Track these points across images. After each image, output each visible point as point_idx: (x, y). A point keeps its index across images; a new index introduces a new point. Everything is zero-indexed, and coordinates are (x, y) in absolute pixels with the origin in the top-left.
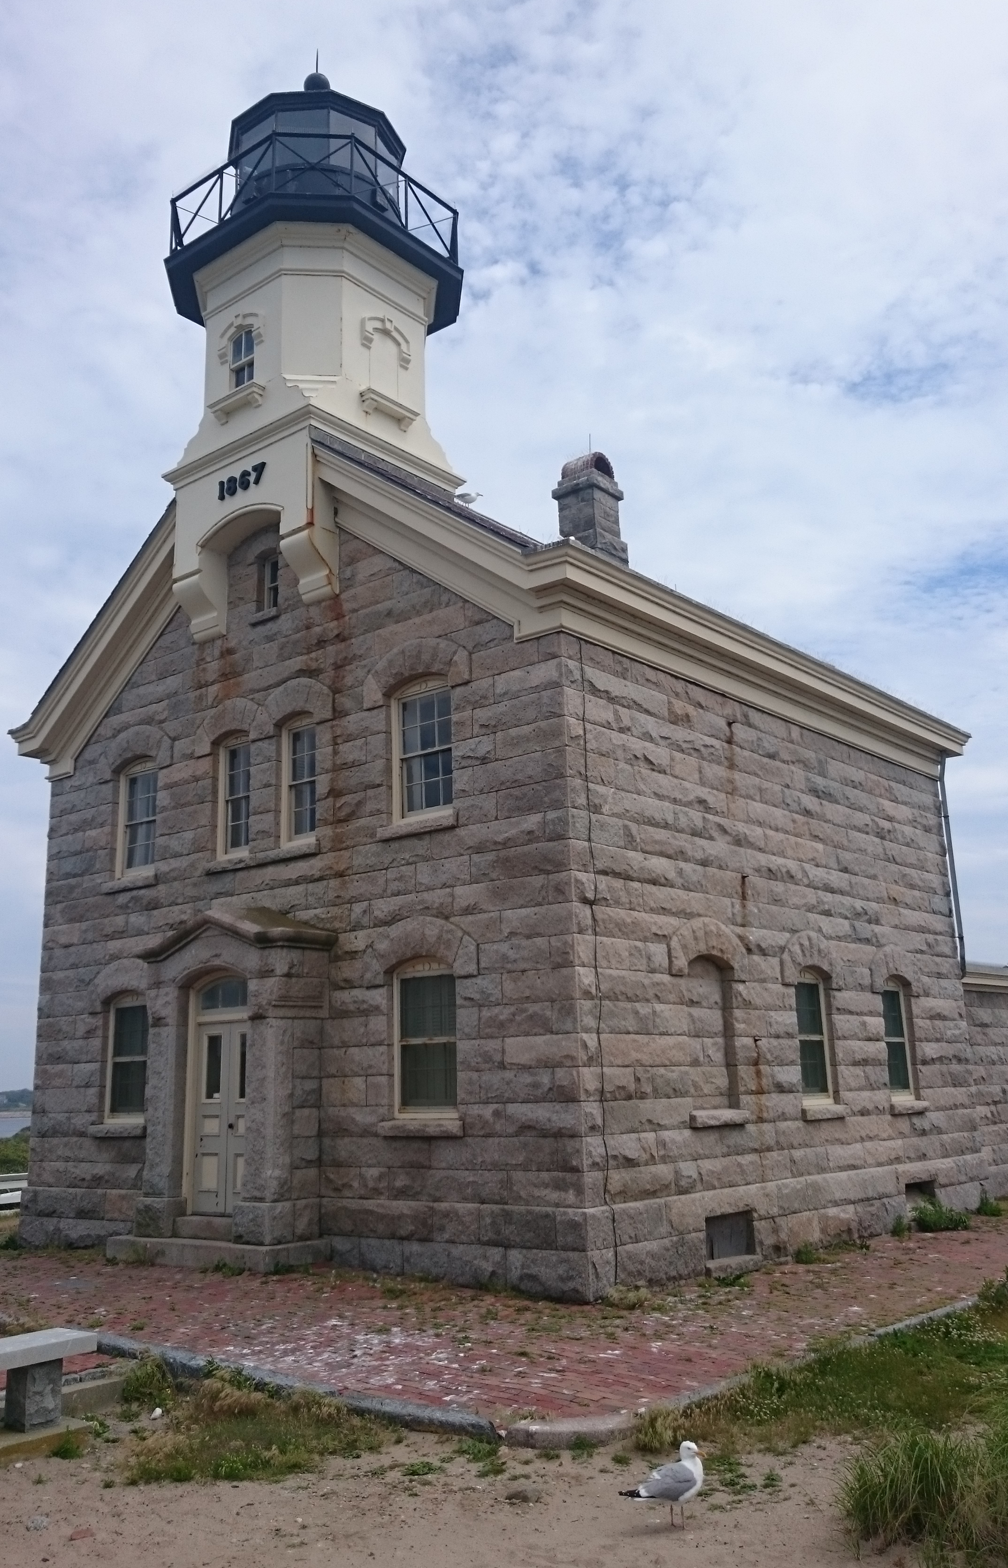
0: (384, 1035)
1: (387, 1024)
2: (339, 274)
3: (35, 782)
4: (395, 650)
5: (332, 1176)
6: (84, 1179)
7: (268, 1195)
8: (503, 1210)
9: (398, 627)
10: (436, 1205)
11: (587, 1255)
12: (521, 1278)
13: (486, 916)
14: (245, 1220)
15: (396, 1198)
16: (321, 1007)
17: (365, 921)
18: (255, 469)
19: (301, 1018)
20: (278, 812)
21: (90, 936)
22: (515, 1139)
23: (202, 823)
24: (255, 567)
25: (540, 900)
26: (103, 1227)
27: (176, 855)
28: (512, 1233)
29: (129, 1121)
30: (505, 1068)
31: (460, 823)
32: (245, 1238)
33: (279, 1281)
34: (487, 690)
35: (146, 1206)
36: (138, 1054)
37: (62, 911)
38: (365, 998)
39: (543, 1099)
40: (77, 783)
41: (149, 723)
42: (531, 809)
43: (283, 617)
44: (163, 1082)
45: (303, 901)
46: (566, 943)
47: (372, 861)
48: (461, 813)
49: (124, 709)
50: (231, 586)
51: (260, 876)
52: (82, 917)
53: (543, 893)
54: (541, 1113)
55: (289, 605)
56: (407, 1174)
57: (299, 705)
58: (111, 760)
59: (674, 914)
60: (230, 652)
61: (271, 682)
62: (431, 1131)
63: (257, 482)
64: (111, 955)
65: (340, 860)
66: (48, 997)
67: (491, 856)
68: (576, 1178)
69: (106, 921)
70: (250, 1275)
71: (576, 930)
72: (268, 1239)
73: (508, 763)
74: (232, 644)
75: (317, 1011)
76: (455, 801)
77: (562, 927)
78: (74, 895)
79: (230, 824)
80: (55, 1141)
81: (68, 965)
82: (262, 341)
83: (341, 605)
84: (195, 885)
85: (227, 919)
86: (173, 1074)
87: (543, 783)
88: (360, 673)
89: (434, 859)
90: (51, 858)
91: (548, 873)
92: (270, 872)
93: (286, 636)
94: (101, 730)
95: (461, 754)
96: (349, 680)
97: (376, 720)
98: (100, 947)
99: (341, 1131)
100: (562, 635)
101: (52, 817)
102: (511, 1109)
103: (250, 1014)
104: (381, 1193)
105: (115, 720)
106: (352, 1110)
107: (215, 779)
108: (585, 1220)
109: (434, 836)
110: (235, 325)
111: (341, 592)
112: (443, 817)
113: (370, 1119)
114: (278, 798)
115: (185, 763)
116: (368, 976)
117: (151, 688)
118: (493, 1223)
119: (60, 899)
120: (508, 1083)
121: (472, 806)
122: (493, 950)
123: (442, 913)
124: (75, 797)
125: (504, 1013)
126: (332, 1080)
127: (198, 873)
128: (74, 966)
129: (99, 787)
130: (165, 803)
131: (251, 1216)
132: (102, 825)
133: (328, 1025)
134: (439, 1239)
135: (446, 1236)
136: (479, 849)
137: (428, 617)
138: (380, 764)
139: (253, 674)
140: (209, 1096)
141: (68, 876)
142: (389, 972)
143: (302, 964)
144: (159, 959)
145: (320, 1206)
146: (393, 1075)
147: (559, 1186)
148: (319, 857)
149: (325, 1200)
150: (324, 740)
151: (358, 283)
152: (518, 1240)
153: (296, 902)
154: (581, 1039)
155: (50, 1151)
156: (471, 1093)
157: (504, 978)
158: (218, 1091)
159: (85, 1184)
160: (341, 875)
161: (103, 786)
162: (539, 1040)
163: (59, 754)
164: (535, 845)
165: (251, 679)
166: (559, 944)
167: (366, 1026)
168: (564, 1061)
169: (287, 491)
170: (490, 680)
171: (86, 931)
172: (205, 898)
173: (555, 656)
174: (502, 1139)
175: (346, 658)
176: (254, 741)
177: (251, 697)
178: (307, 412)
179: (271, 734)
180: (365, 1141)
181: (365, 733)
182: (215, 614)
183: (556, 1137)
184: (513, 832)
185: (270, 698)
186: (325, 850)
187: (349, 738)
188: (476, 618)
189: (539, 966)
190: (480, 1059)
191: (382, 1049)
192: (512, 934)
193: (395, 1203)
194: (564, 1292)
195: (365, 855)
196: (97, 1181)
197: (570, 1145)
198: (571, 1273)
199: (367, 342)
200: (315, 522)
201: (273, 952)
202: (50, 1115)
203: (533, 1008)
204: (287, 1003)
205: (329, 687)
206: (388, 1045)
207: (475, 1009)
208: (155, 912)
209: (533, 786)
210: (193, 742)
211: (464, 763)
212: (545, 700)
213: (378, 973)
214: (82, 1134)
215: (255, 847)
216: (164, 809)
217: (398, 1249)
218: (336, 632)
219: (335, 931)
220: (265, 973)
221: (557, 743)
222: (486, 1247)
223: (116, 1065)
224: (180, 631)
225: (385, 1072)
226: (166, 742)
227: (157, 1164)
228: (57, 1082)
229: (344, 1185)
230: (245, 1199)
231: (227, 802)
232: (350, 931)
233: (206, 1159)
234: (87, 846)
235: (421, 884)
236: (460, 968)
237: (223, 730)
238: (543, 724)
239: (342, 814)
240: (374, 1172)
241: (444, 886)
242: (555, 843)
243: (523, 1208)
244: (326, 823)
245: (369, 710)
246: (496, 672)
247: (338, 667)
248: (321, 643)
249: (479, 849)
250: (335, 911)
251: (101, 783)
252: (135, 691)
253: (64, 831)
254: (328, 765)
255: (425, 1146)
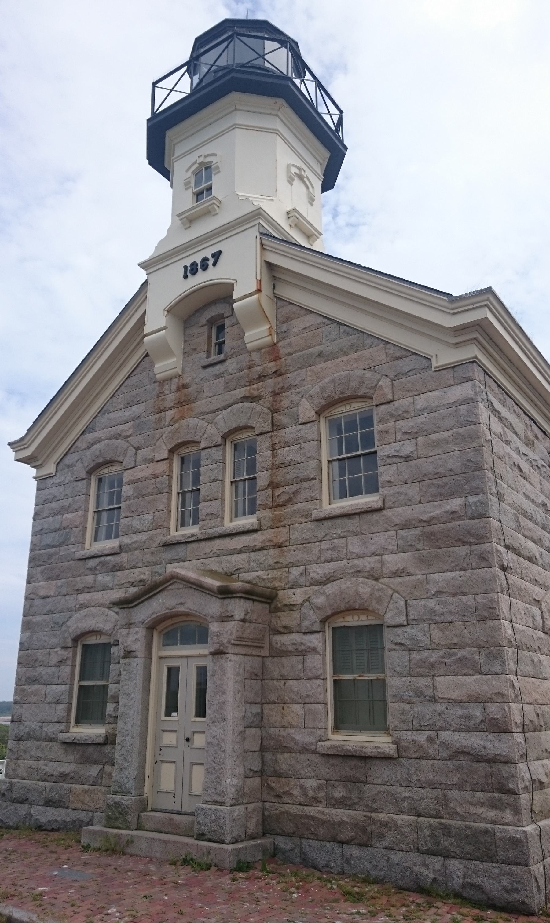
0: (320, 672)
1: (323, 663)
2: (275, 132)
3: (25, 480)
4: (326, 380)
5: (273, 785)
6: (52, 775)
7: (228, 799)
8: (441, 824)
9: (329, 364)
10: (373, 815)
11: (530, 870)
12: (464, 886)
13: (413, 578)
14: (207, 820)
15: (334, 806)
16: (262, 647)
17: (302, 581)
18: (213, 255)
19: (249, 655)
20: (223, 500)
21: (64, 591)
22: (449, 762)
23: (160, 508)
24: (205, 329)
25: (465, 565)
26: (68, 814)
27: (137, 532)
28: (451, 844)
29: (94, 731)
30: (435, 701)
31: (387, 506)
32: (208, 836)
33: (247, 879)
34: (409, 406)
35: (116, 803)
36: (99, 680)
37: (42, 572)
38: (303, 641)
39: (475, 729)
40: (58, 481)
41: (117, 438)
42: (453, 495)
43: (229, 361)
44: (132, 702)
45: (246, 565)
46: (492, 600)
47: (308, 535)
48: (387, 499)
49: (97, 429)
50: (185, 341)
51: (207, 547)
52: (58, 576)
53: (467, 560)
54: (475, 741)
55: (234, 352)
56: (344, 786)
57: (242, 422)
58: (86, 464)
59: (540, 586)
60: (185, 386)
61: (219, 406)
62: (368, 752)
63: (214, 264)
64: (81, 604)
65: (281, 535)
66: (28, 635)
67: (417, 532)
68: (512, 799)
69: (79, 579)
70: (218, 870)
71: (499, 589)
72: (228, 839)
73: (429, 460)
74: (187, 380)
75: (264, 649)
76: (381, 490)
77: (487, 587)
78: (52, 560)
79: (180, 510)
80: (30, 744)
81: (45, 611)
82: (219, 172)
83: (278, 350)
84: (152, 553)
85: (192, 575)
86: (141, 696)
87: (463, 475)
88: (295, 398)
89: (363, 534)
90: (34, 534)
91: (470, 544)
92: (217, 544)
93: (231, 374)
94: (78, 444)
95: (386, 454)
96: (285, 403)
97: (309, 431)
98: (72, 598)
99: (282, 747)
100: (475, 364)
101: (36, 505)
102: (445, 736)
103: (212, 650)
104: (320, 802)
105: (90, 437)
106: (291, 731)
107: (170, 477)
108: (526, 837)
109: (363, 516)
110: (198, 162)
111: (277, 342)
112: (373, 501)
113: (309, 739)
114: (223, 491)
115: (147, 465)
116: (306, 623)
117: (120, 414)
118: (432, 835)
119: (41, 563)
120: (440, 714)
121: (398, 493)
122: (419, 607)
123: (372, 576)
124: (55, 491)
125: (434, 657)
126: (270, 706)
127: (156, 544)
128: (50, 612)
129: (76, 483)
130: (130, 494)
131: (213, 818)
132: (77, 510)
133: (269, 662)
134: (378, 845)
135: (386, 843)
136: (405, 526)
137: (355, 356)
138: (313, 463)
139: (203, 401)
140: (168, 714)
141: (48, 546)
142: (323, 622)
143: (252, 611)
144: (130, 606)
145: (264, 809)
146: (326, 704)
147: (494, 805)
148: (259, 533)
149: (267, 805)
150: (264, 447)
151: (285, 141)
152: (458, 851)
153: (241, 566)
154: (510, 680)
155: (25, 752)
156: (404, 721)
157: (432, 628)
158: (176, 711)
159: (54, 779)
160: (280, 546)
161: (79, 483)
162: (470, 679)
163: (44, 461)
164: (458, 523)
165: (201, 405)
166: (485, 601)
167: (303, 663)
168: (495, 697)
169: (241, 269)
170: (411, 400)
171: (61, 586)
172: (161, 563)
173: (469, 380)
174: (436, 762)
175: (283, 387)
176: (204, 449)
177: (202, 417)
178: (258, 213)
179: (219, 443)
180: (304, 757)
181: (300, 440)
182: (175, 359)
183: (489, 763)
184: (437, 512)
185: (218, 417)
186: (265, 528)
187: (286, 445)
188: (398, 354)
189: (466, 619)
190: (411, 694)
191: (318, 682)
192: (439, 592)
193: (334, 811)
194: (509, 903)
195: (301, 530)
196: (64, 777)
197: (505, 770)
198: (516, 886)
199: (290, 181)
200: (262, 289)
201: (232, 601)
202: (26, 724)
203: (460, 653)
204: (241, 643)
205: (269, 408)
206: (324, 679)
207: (405, 653)
208: (119, 573)
209: (454, 477)
210: (153, 450)
211: (389, 461)
212: (462, 412)
213: (316, 622)
214: (52, 740)
215: (204, 525)
216: (128, 498)
217: (338, 850)
218: (274, 369)
219: (275, 589)
220: (225, 618)
221: (475, 444)
222: (425, 856)
223: (81, 687)
224: (144, 374)
225: (321, 701)
226: (131, 451)
227: (125, 768)
228: (33, 699)
229: (284, 793)
230: (206, 802)
231: (178, 494)
232: (288, 589)
233: (164, 765)
234: (64, 525)
235: (352, 553)
236: (389, 618)
237: (179, 441)
238: (461, 430)
239: (280, 501)
240: (311, 784)
241: (373, 554)
242: (476, 521)
243: (460, 822)
244: (265, 507)
245: (303, 424)
246: (416, 393)
247: (275, 394)
248: (262, 377)
249: (405, 526)
250: (276, 573)
251: (77, 481)
252: (106, 416)
253: (46, 515)
254: (268, 464)
255: (361, 764)
